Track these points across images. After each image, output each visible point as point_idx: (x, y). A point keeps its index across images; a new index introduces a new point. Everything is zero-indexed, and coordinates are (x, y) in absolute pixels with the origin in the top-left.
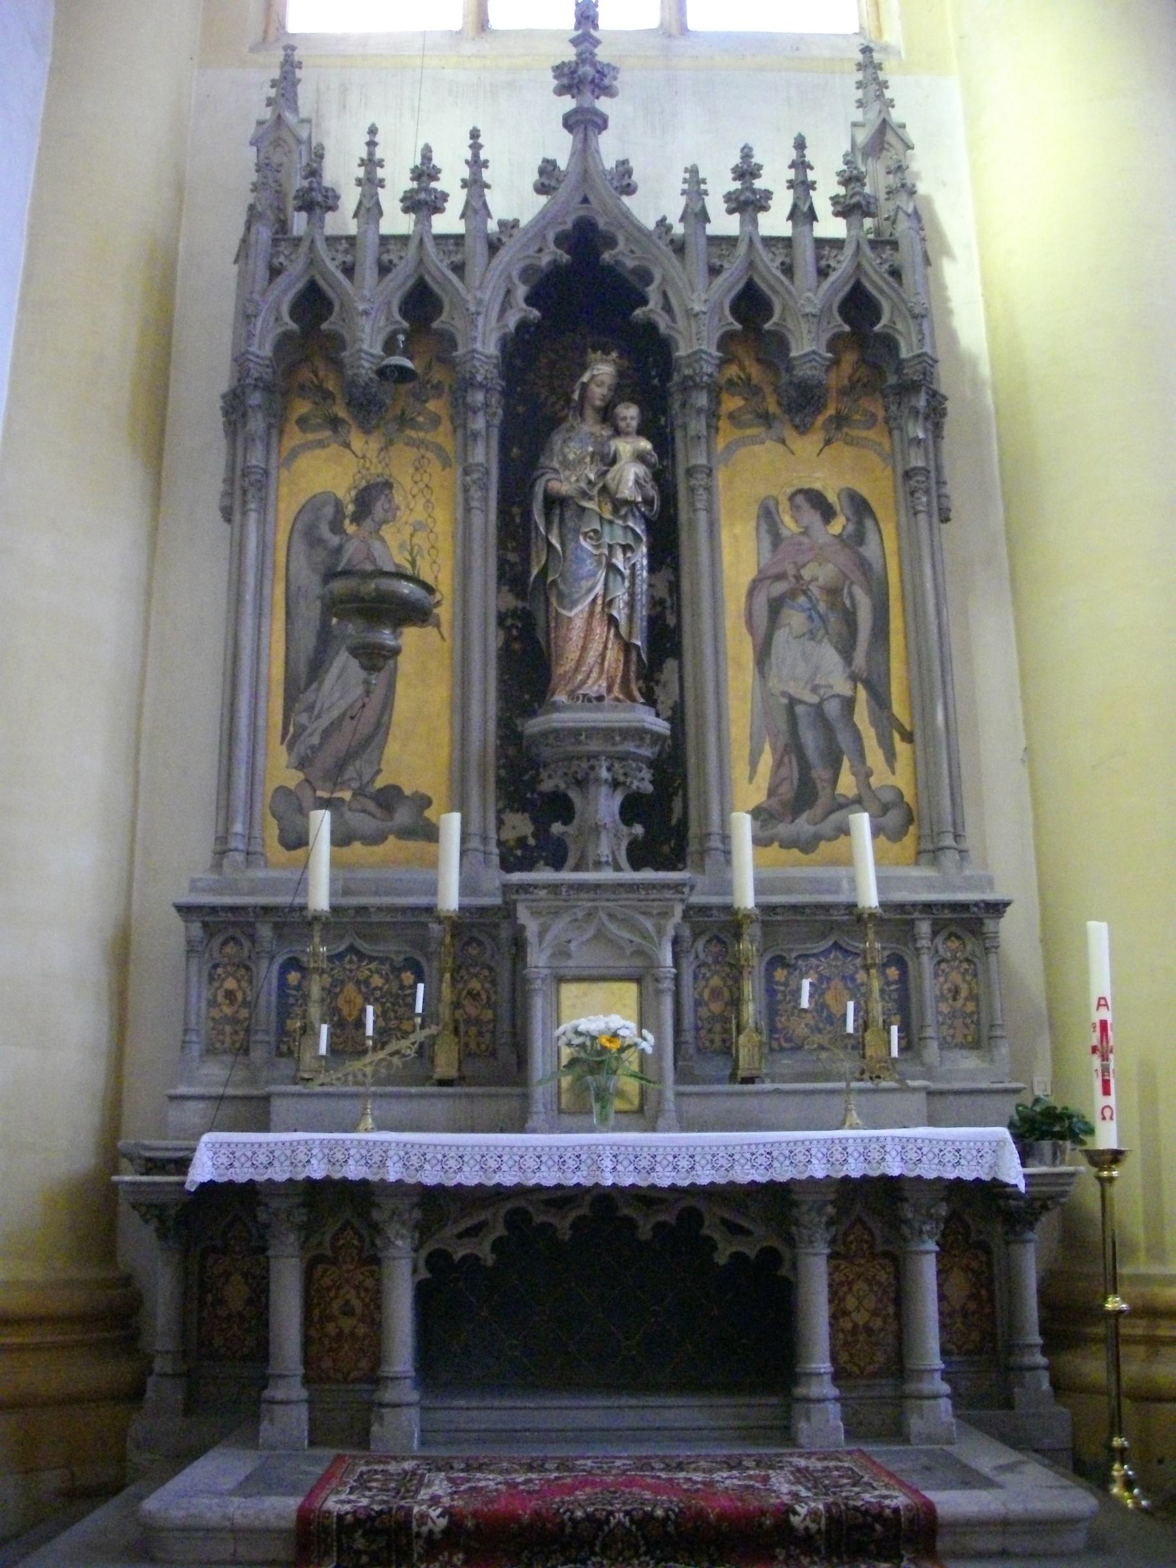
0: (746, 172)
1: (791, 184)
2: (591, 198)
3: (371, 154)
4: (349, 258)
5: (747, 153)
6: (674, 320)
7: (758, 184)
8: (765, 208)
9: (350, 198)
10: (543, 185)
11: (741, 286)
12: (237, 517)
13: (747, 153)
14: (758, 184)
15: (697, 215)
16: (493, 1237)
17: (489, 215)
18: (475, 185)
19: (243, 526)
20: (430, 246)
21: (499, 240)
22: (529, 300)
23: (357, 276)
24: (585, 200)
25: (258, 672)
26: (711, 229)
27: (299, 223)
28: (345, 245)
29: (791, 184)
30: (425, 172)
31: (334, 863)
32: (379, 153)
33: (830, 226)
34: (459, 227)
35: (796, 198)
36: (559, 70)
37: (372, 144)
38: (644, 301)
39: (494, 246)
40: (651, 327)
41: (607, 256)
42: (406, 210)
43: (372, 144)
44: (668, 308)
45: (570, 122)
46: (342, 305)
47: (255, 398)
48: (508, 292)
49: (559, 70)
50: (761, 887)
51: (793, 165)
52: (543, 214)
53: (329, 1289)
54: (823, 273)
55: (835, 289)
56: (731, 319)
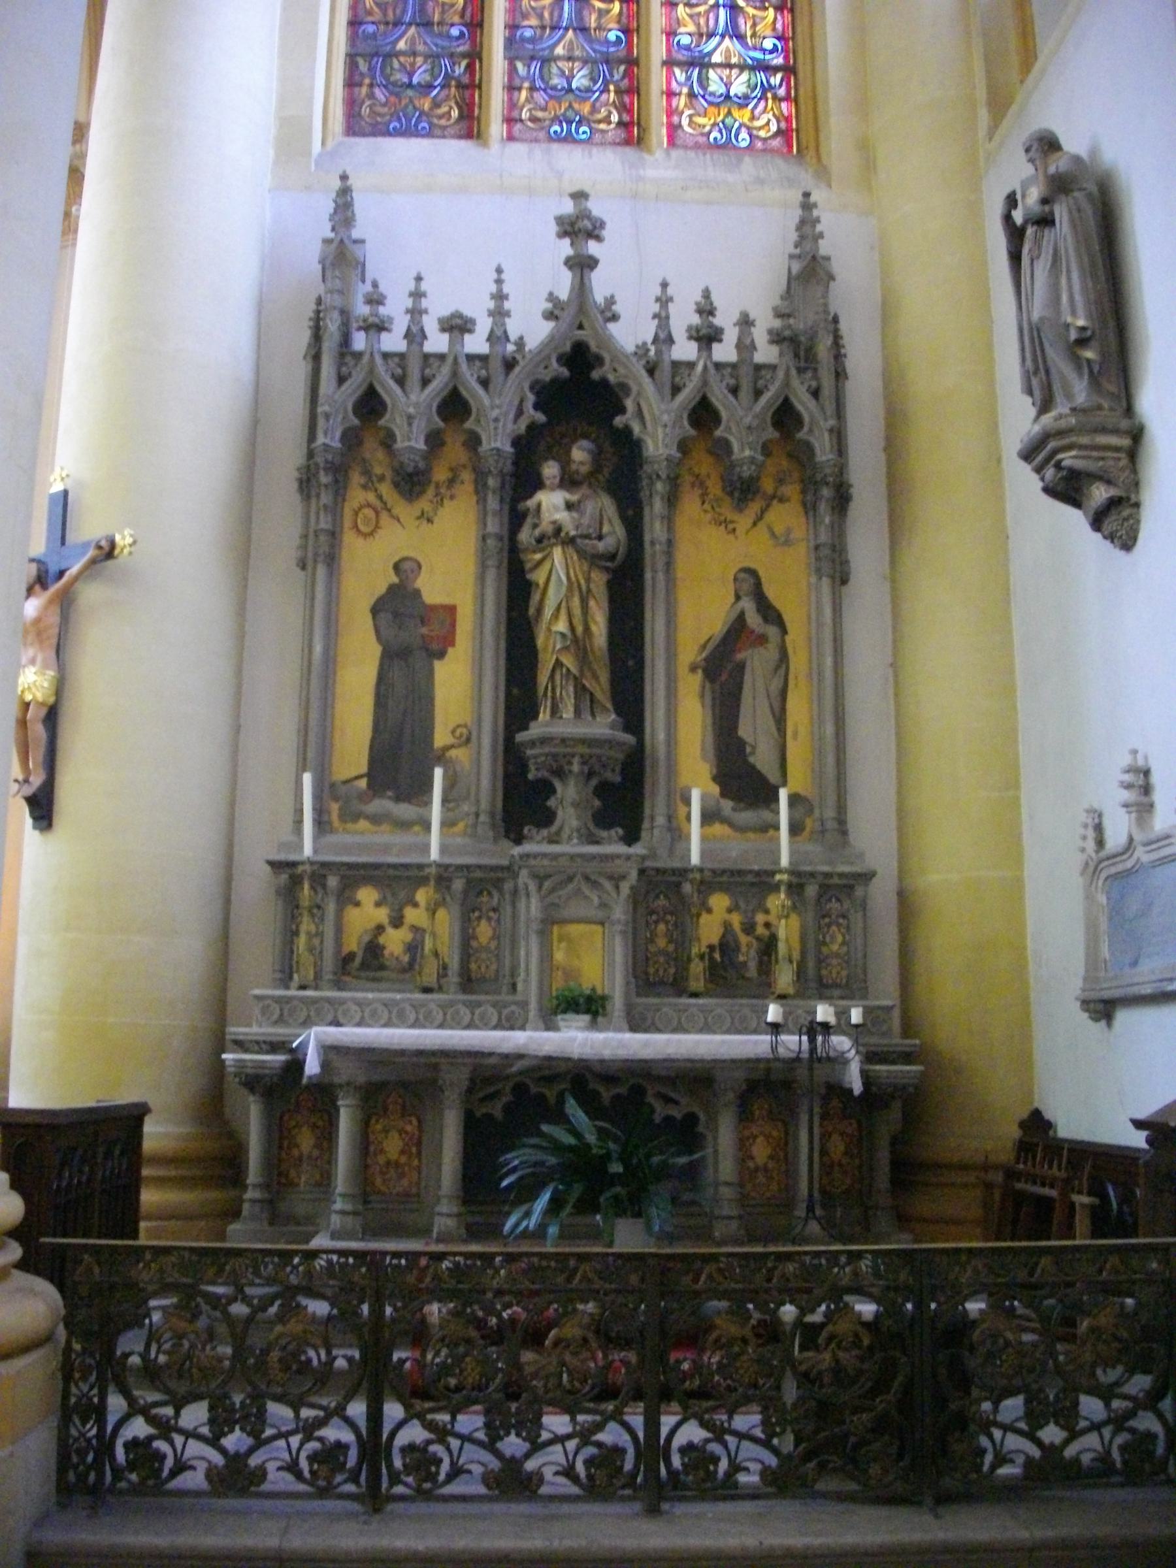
0: (706, 310)
1: (491, 313)
2: (586, 325)
3: (417, 287)
4: (484, 372)
5: (707, 294)
6: (645, 427)
7: (382, 310)
8: (470, 331)
9: (401, 324)
10: (552, 313)
11: (697, 399)
12: (309, 568)
13: (707, 294)
14: (382, 310)
15: (665, 339)
16: (618, 1090)
17: (507, 339)
18: (499, 314)
19: (314, 574)
20: (378, 360)
21: (514, 358)
22: (536, 407)
23: (491, 386)
24: (581, 327)
25: (819, 706)
26: (429, 347)
27: (359, 341)
28: (396, 360)
29: (491, 313)
30: (706, 310)
31: (704, 839)
32: (506, 289)
33: (765, 353)
34: (401, 346)
35: (495, 323)
36: (560, 220)
37: (499, 282)
38: (622, 410)
39: (509, 364)
40: (627, 430)
41: (595, 375)
42: (772, 342)
43: (499, 282)
44: (640, 414)
45: (570, 263)
46: (393, 405)
47: (324, 478)
48: (522, 401)
49: (560, 220)
50: (703, 854)
51: (411, 294)
52: (551, 338)
53: (748, 1138)
54: (758, 393)
55: (769, 404)
56: (437, 419)
